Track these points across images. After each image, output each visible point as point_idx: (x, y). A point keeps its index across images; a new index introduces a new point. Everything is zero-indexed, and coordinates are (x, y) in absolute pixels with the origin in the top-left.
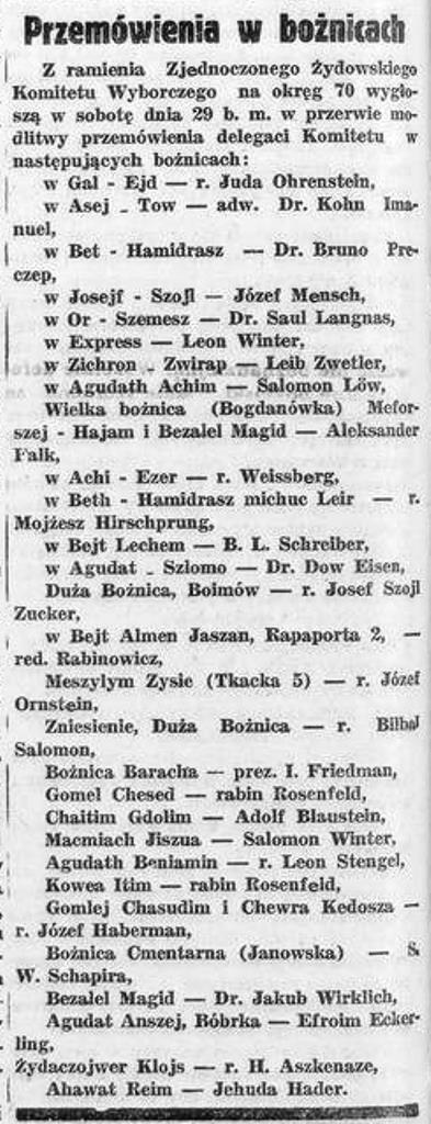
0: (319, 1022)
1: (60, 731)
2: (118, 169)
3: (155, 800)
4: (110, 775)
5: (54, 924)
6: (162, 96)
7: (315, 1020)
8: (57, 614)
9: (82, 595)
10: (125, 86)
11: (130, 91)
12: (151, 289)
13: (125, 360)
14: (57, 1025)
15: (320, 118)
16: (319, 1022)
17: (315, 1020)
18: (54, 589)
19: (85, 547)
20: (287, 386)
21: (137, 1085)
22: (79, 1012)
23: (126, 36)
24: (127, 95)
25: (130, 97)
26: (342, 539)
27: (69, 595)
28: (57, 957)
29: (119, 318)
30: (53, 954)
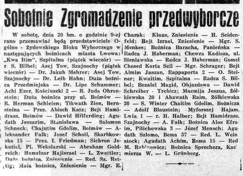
0: (232, 122)
1: (45, 167)
2: (89, 50)
3: (100, 74)
4: (53, 35)
5: (105, 58)
6: (202, 148)
7: (231, 122)
8: (138, 48)
9: (100, 80)
10: (86, 46)
11: (88, 47)
12: (124, 89)
13: (115, 89)
14: (111, 117)
15: (24, 42)
16: (232, 122)
17: (231, 122)
18: (26, 97)
19: (95, 110)
20: (36, 48)
21: (231, 140)
22: (179, 151)
23: (82, 13)
24: (87, 48)
25: (87, 48)
26: (142, 90)
27: (96, 80)
28: (94, 98)
29: (141, 134)
30: (93, 97)
